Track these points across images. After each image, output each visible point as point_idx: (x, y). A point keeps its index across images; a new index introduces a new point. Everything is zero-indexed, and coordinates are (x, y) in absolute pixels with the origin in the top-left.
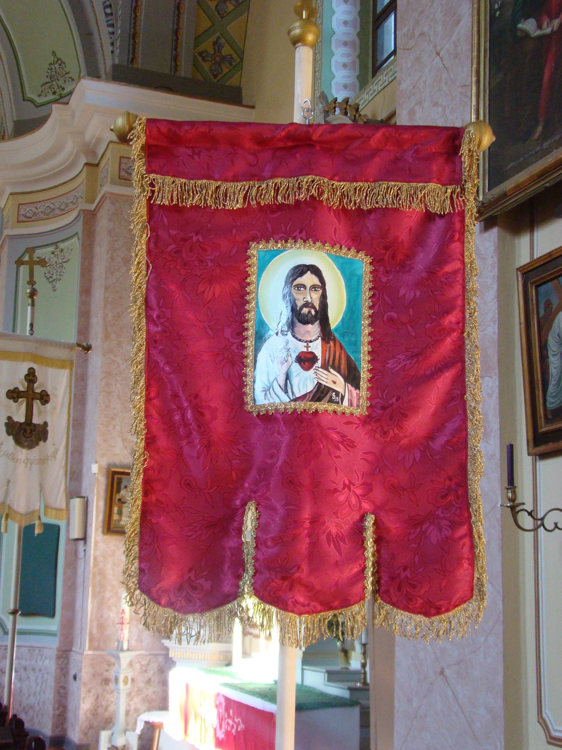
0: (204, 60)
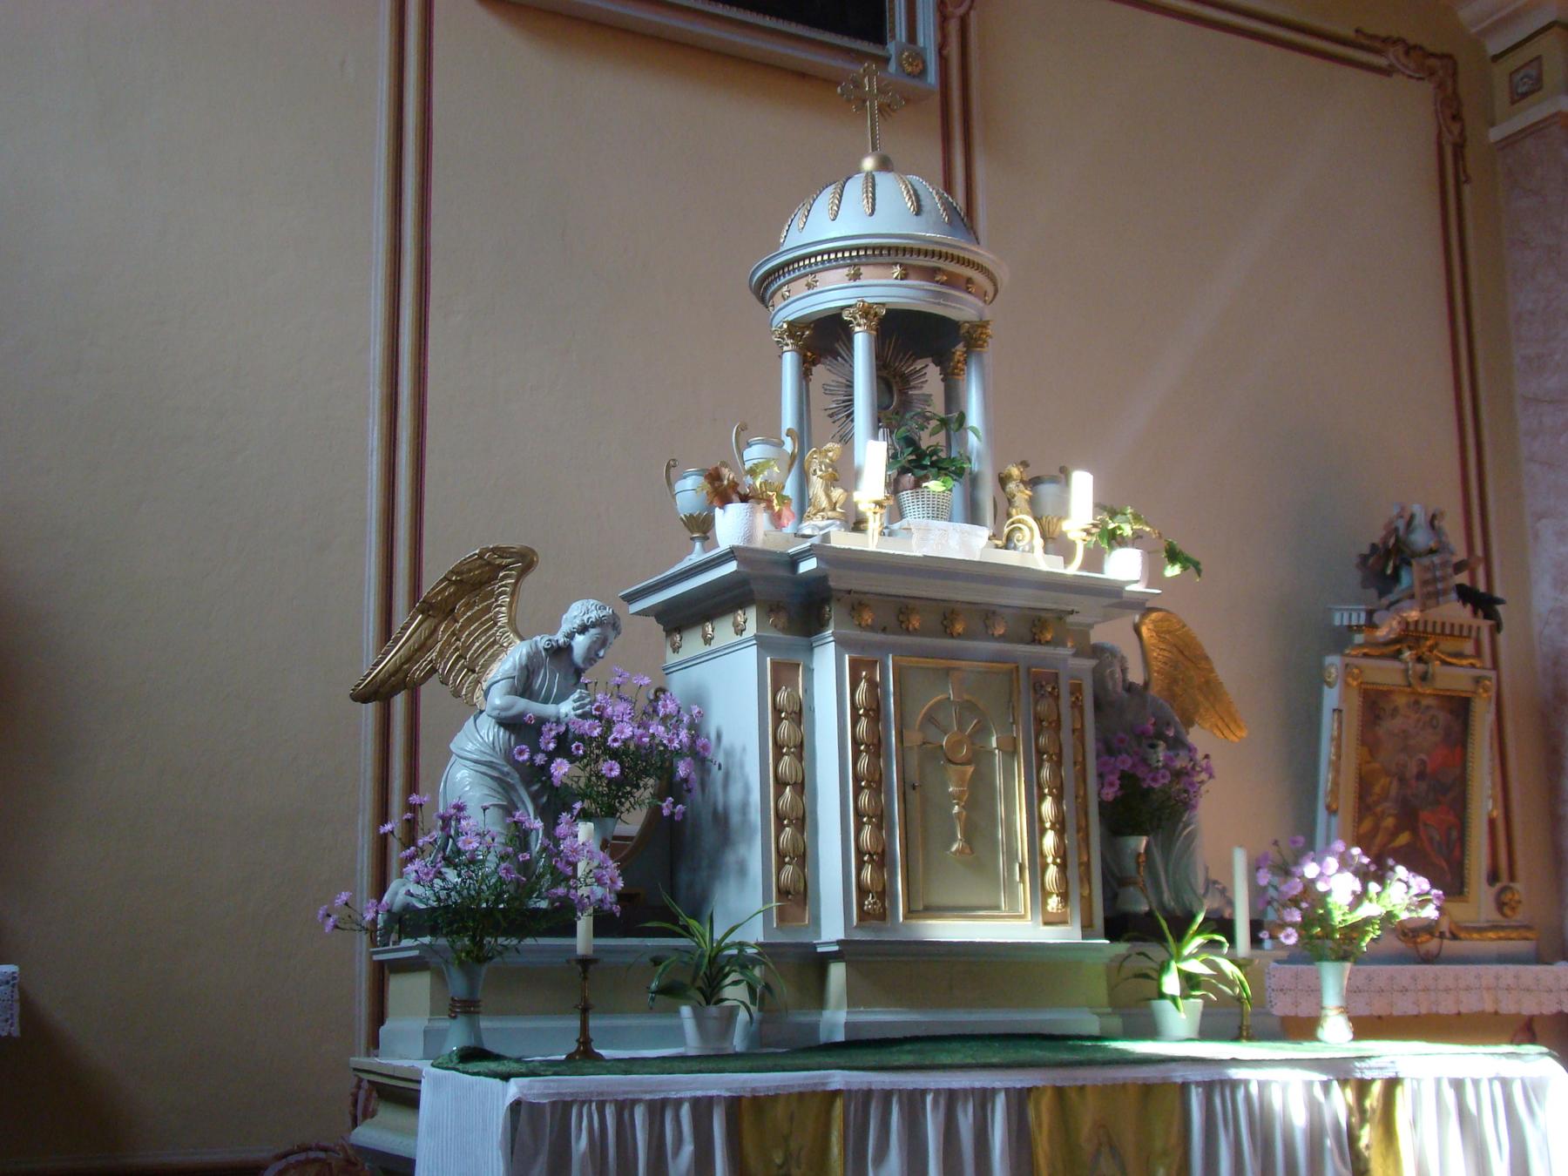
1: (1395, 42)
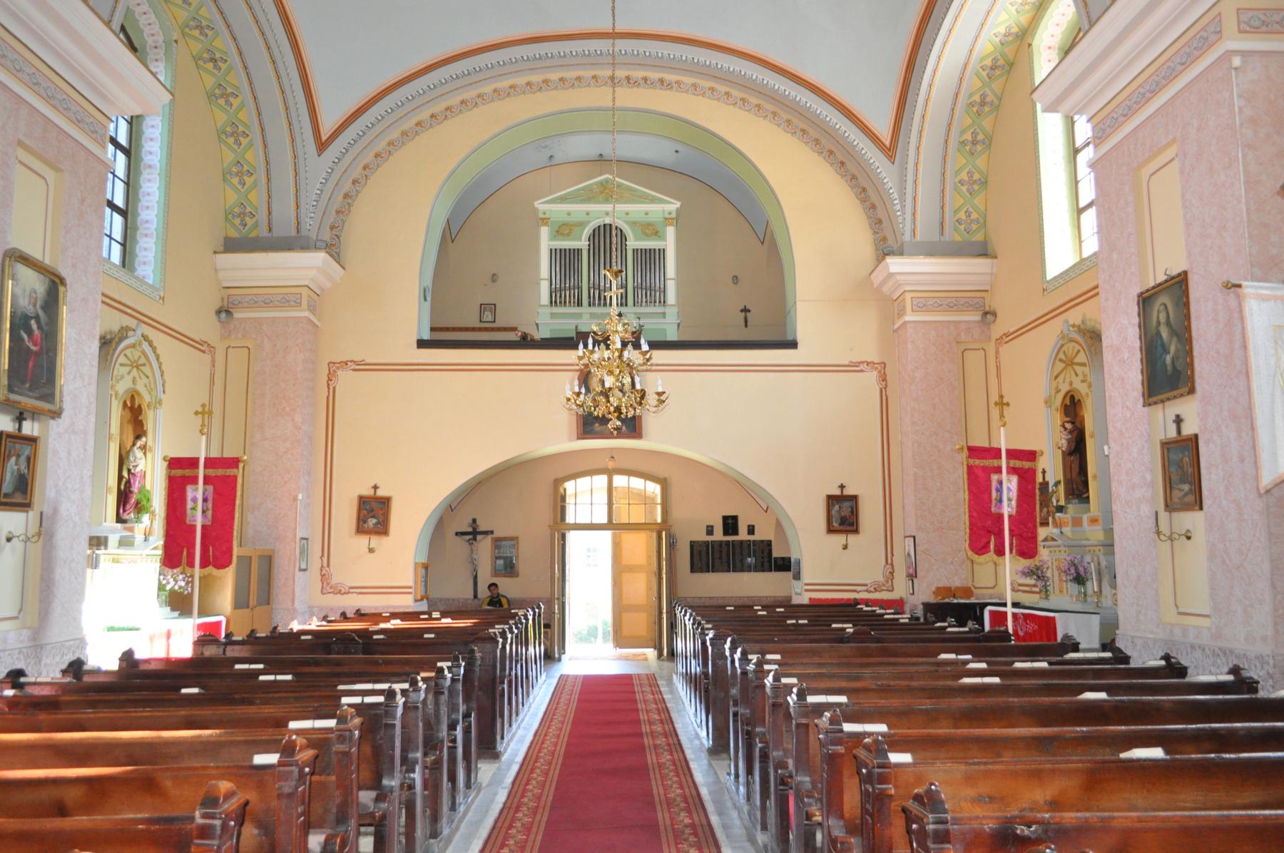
0: (960, 224)
1: (863, 362)
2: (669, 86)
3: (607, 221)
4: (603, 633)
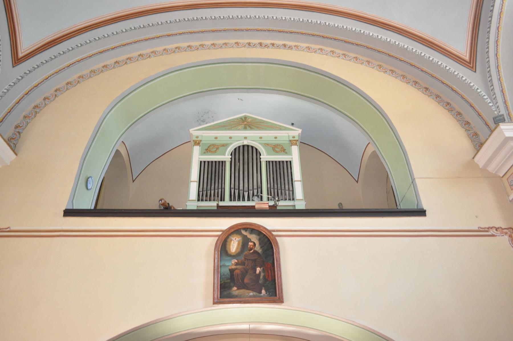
1: (492, 228)
2: (290, 48)
3: (246, 143)
4: (245, 128)
